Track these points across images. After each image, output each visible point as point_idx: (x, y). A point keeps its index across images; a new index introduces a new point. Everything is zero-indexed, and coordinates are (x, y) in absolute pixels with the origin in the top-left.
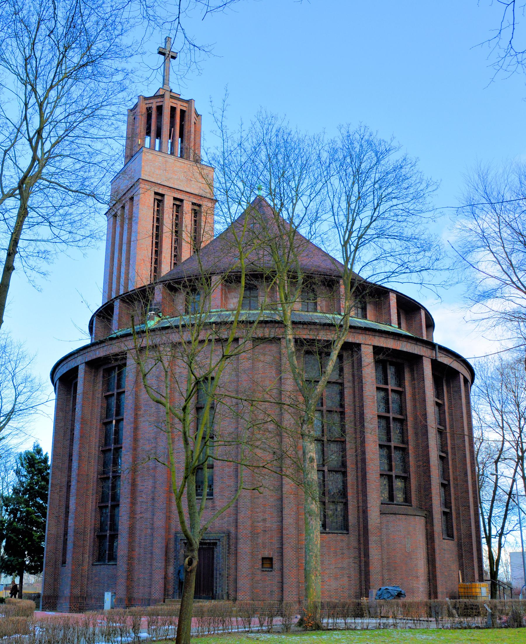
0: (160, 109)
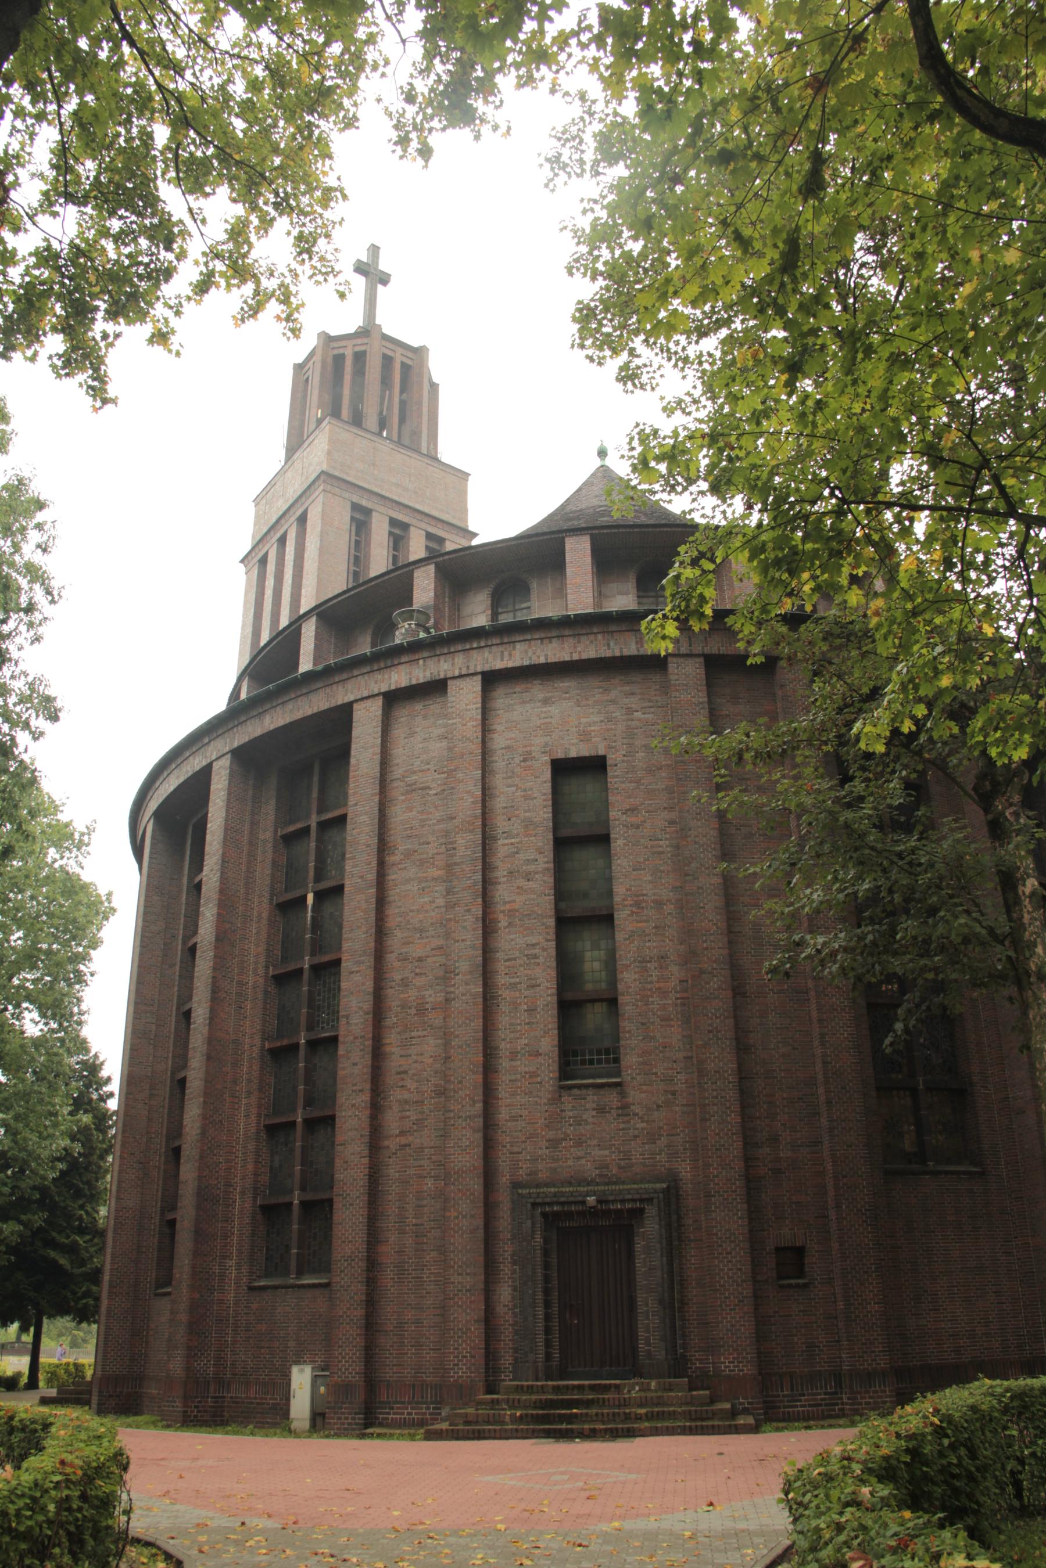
0: (360, 358)
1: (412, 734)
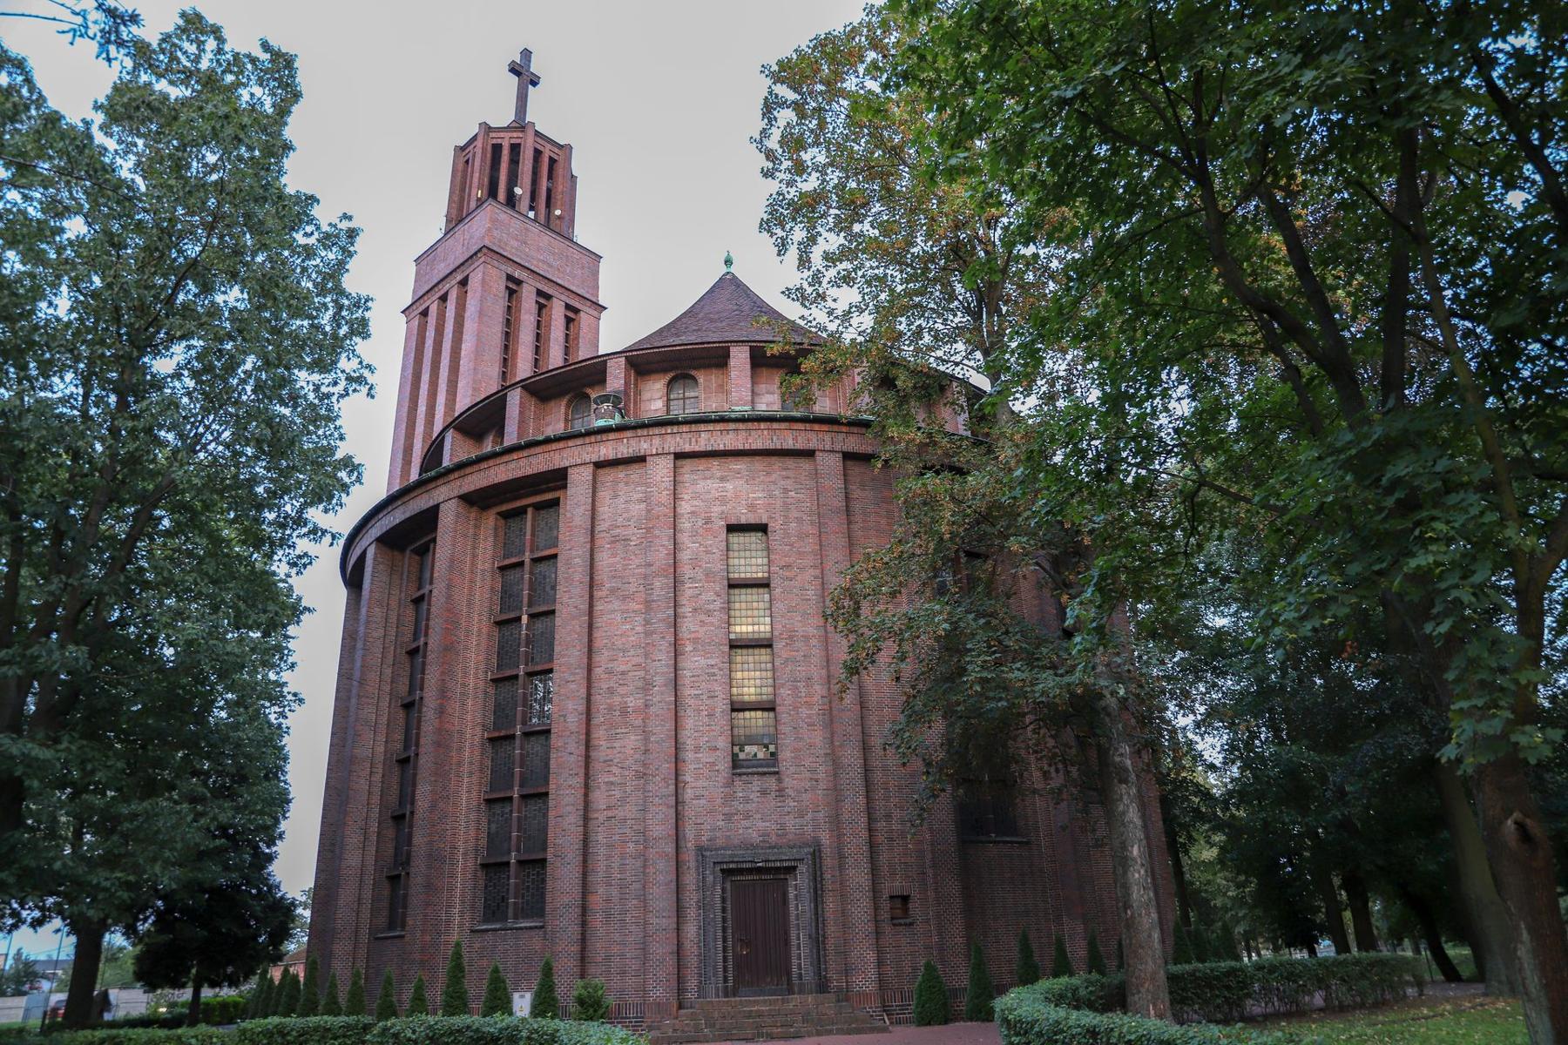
0: (515, 149)
1: (616, 496)
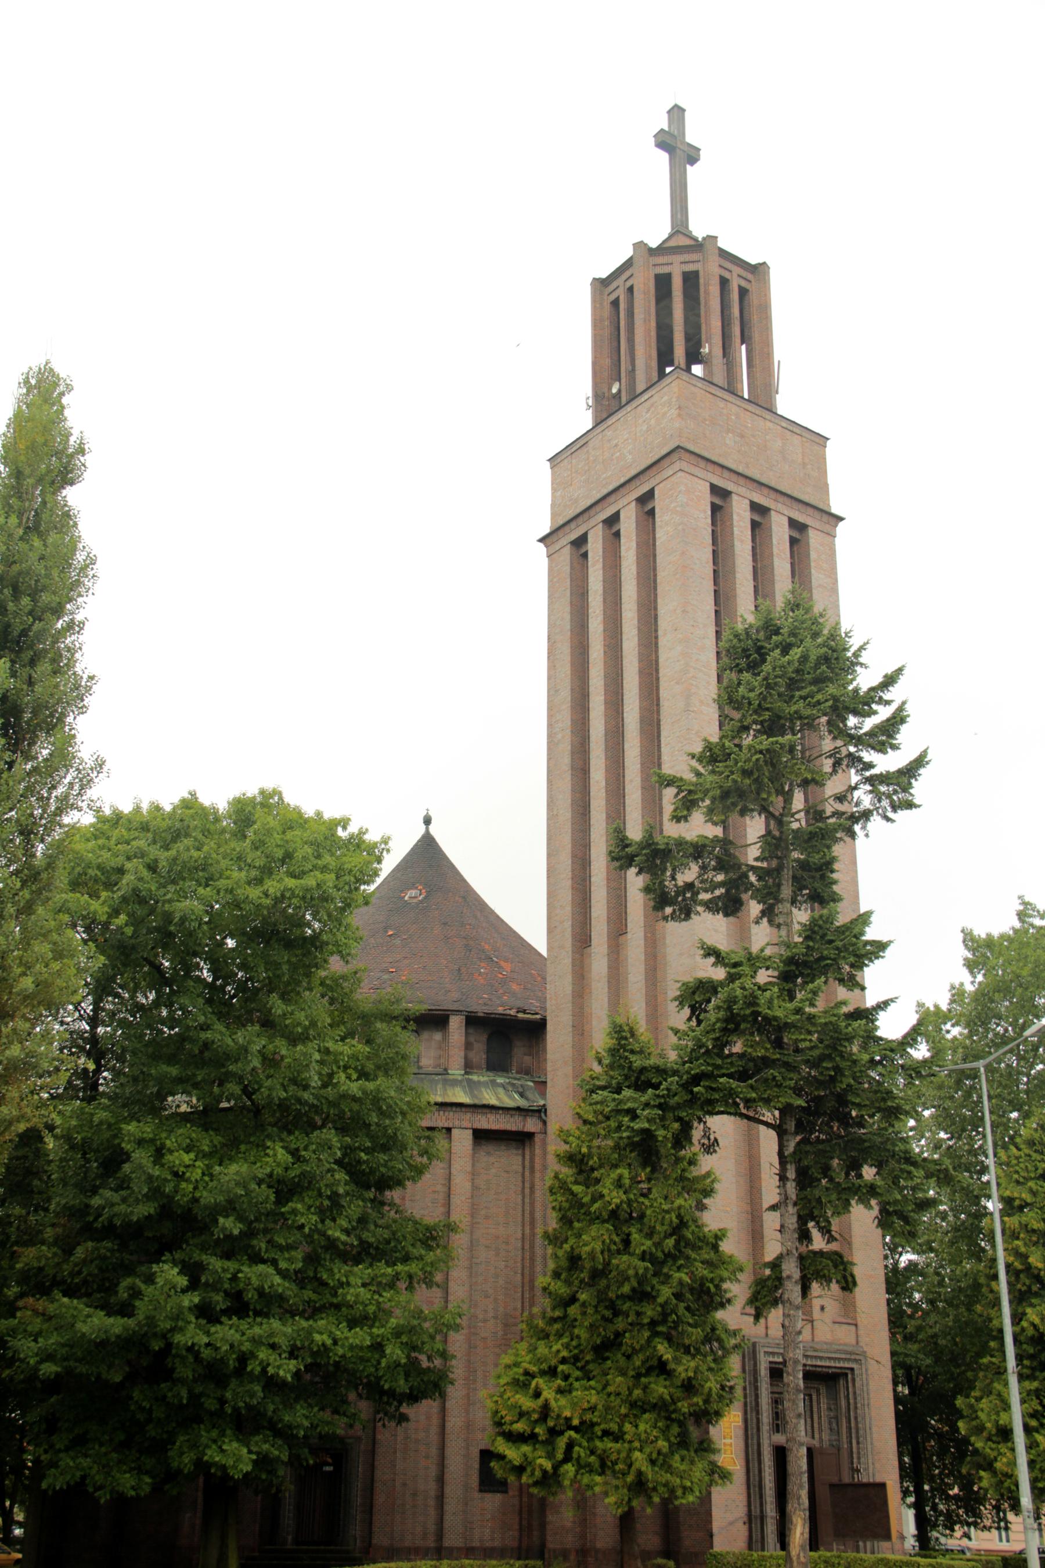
0: (691, 280)
